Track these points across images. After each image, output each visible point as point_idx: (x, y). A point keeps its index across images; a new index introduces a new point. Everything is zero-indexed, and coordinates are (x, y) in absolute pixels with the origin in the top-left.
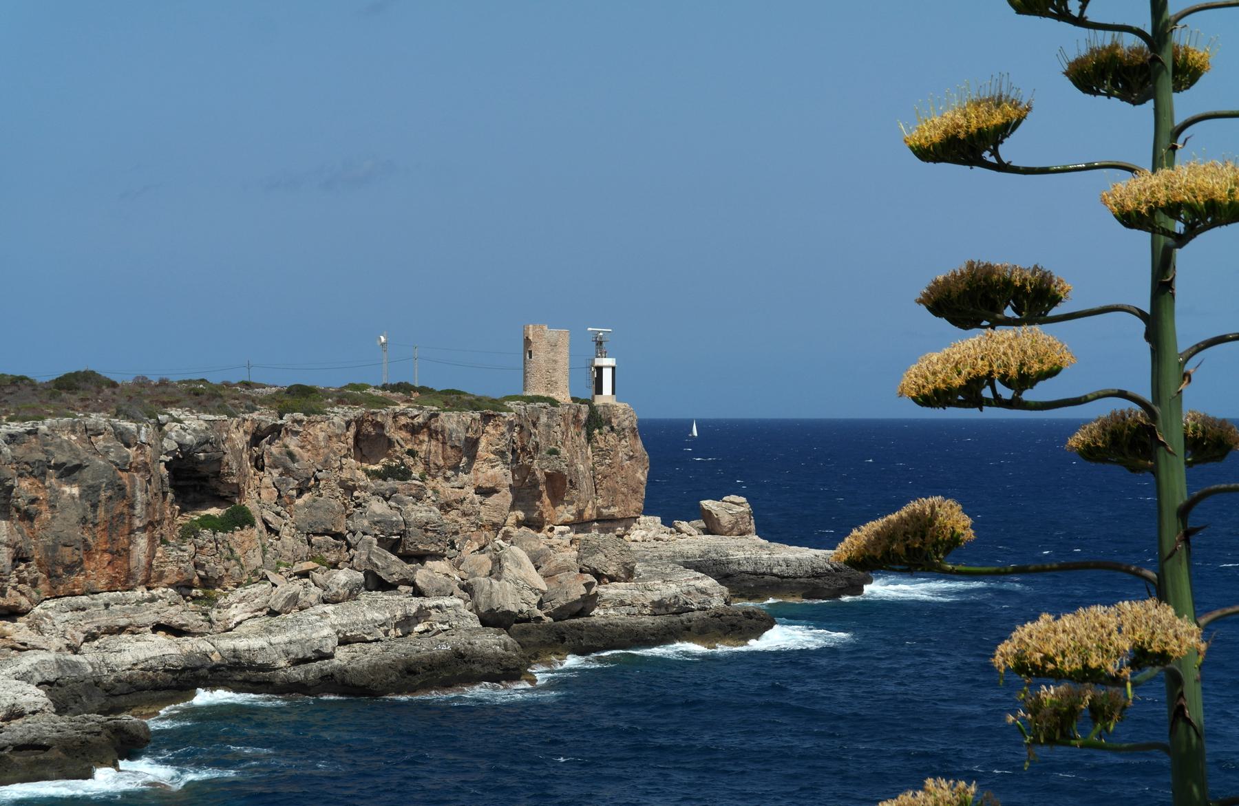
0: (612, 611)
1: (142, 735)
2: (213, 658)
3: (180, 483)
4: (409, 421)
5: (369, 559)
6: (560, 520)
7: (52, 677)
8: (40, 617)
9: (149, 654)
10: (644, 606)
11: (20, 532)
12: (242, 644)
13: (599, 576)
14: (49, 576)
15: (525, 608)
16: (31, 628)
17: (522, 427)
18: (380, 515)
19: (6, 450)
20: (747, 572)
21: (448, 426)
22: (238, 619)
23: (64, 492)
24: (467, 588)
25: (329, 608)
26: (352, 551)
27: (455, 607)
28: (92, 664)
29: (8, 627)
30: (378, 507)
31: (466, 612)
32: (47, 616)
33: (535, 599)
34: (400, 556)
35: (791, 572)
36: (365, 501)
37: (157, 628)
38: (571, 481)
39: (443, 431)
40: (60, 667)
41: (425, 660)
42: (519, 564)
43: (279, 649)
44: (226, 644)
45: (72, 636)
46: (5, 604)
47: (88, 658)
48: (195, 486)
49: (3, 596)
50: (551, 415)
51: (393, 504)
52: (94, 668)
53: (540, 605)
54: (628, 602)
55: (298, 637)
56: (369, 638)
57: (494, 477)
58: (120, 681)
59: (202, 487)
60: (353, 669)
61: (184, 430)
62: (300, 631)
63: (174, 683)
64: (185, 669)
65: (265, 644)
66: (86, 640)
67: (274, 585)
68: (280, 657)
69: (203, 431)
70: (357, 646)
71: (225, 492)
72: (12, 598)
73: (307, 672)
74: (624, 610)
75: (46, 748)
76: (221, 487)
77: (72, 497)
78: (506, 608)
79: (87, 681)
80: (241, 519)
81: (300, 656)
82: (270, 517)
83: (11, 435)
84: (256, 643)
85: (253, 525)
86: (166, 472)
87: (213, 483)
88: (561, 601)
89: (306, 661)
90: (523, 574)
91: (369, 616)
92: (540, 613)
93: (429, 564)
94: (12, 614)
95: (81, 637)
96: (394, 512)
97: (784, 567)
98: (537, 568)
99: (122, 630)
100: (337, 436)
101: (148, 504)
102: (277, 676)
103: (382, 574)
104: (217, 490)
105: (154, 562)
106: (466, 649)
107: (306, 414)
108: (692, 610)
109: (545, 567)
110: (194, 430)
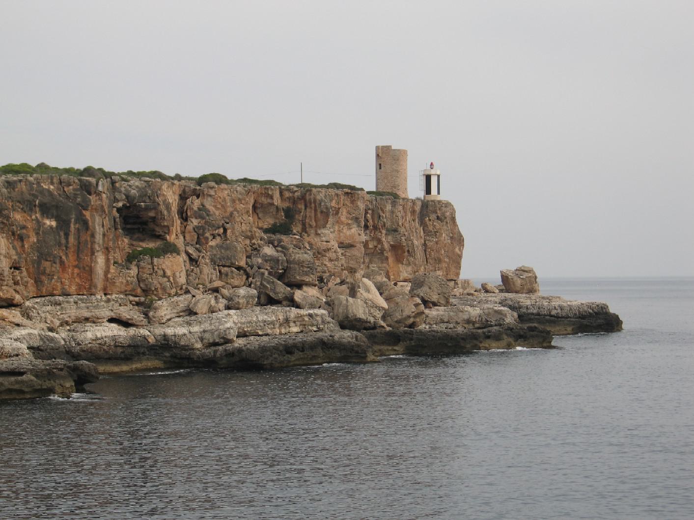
0: (434, 326)
1: (93, 373)
2: (150, 340)
3: (129, 226)
4: (291, 195)
5: (261, 284)
6: (401, 278)
7: (36, 345)
8: (29, 308)
9: (104, 334)
10: (457, 323)
11: (14, 248)
12: (170, 331)
13: (425, 302)
14: (36, 282)
15: (372, 320)
16: (23, 316)
17: (373, 211)
18: (270, 256)
19: (4, 190)
20: (533, 314)
21: (318, 198)
22: (168, 317)
23: (45, 224)
24: (329, 304)
25: (232, 312)
26: (250, 279)
27: (322, 316)
28: (64, 339)
29: (4, 312)
30: (269, 251)
31: (329, 319)
32: (34, 308)
33: (379, 314)
34: (284, 283)
35: (564, 314)
36: (260, 246)
37: (111, 320)
38: (408, 251)
39: (315, 201)
40: (42, 339)
41: (299, 345)
42: (368, 290)
43: (196, 336)
44: (159, 331)
45: (52, 321)
46: (4, 297)
47: (61, 336)
48: (139, 229)
49: (1, 290)
50: (394, 204)
51: (280, 249)
52: (66, 342)
53: (384, 318)
54: (446, 320)
55: (209, 328)
56: (260, 333)
57: (352, 236)
58: (84, 351)
59: (144, 229)
60: (248, 349)
61: (130, 186)
62: (211, 324)
63: (122, 356)
64: (129, 346)
65: (186, 332)
66: (61, 325)
67: (194, 296)
68: (197, 341)
69: (143, 188)
70: (252, 338)
71: (159, 231)
72: (7, 292)
73: (215, 352)
74: (444, 326)
75: (21, 374)
76: (157, 229)
77: (51, 227)
78: (358, 316)
79: (61, 350)
80: (170, 249)
81: (211, 341)
82: (191, 250)
83: (8, 182)
84: (181, 331)
85: (178, 254)
86: (118, 215)
87: (151, 225)
88: (398, 316)
89: (215, 344)
90: (370, 297)
91: (261, 318)
92: (382, 323)
93: (305, 288)
94: (10, 304)
95: (57, 323)
96: (280, 254)
97: (559, 311)
98: (381, 294)
99: (87, 319)
100: (240, 200)
101: (104, 235)
102: (195, 354)
103: (272, 294)
104: (154, 230)
105: (109, 276)
106: (328, 339)
107: (217, 183)
108: (491, 326)
109: (386, 293)
110: (137, 187)
